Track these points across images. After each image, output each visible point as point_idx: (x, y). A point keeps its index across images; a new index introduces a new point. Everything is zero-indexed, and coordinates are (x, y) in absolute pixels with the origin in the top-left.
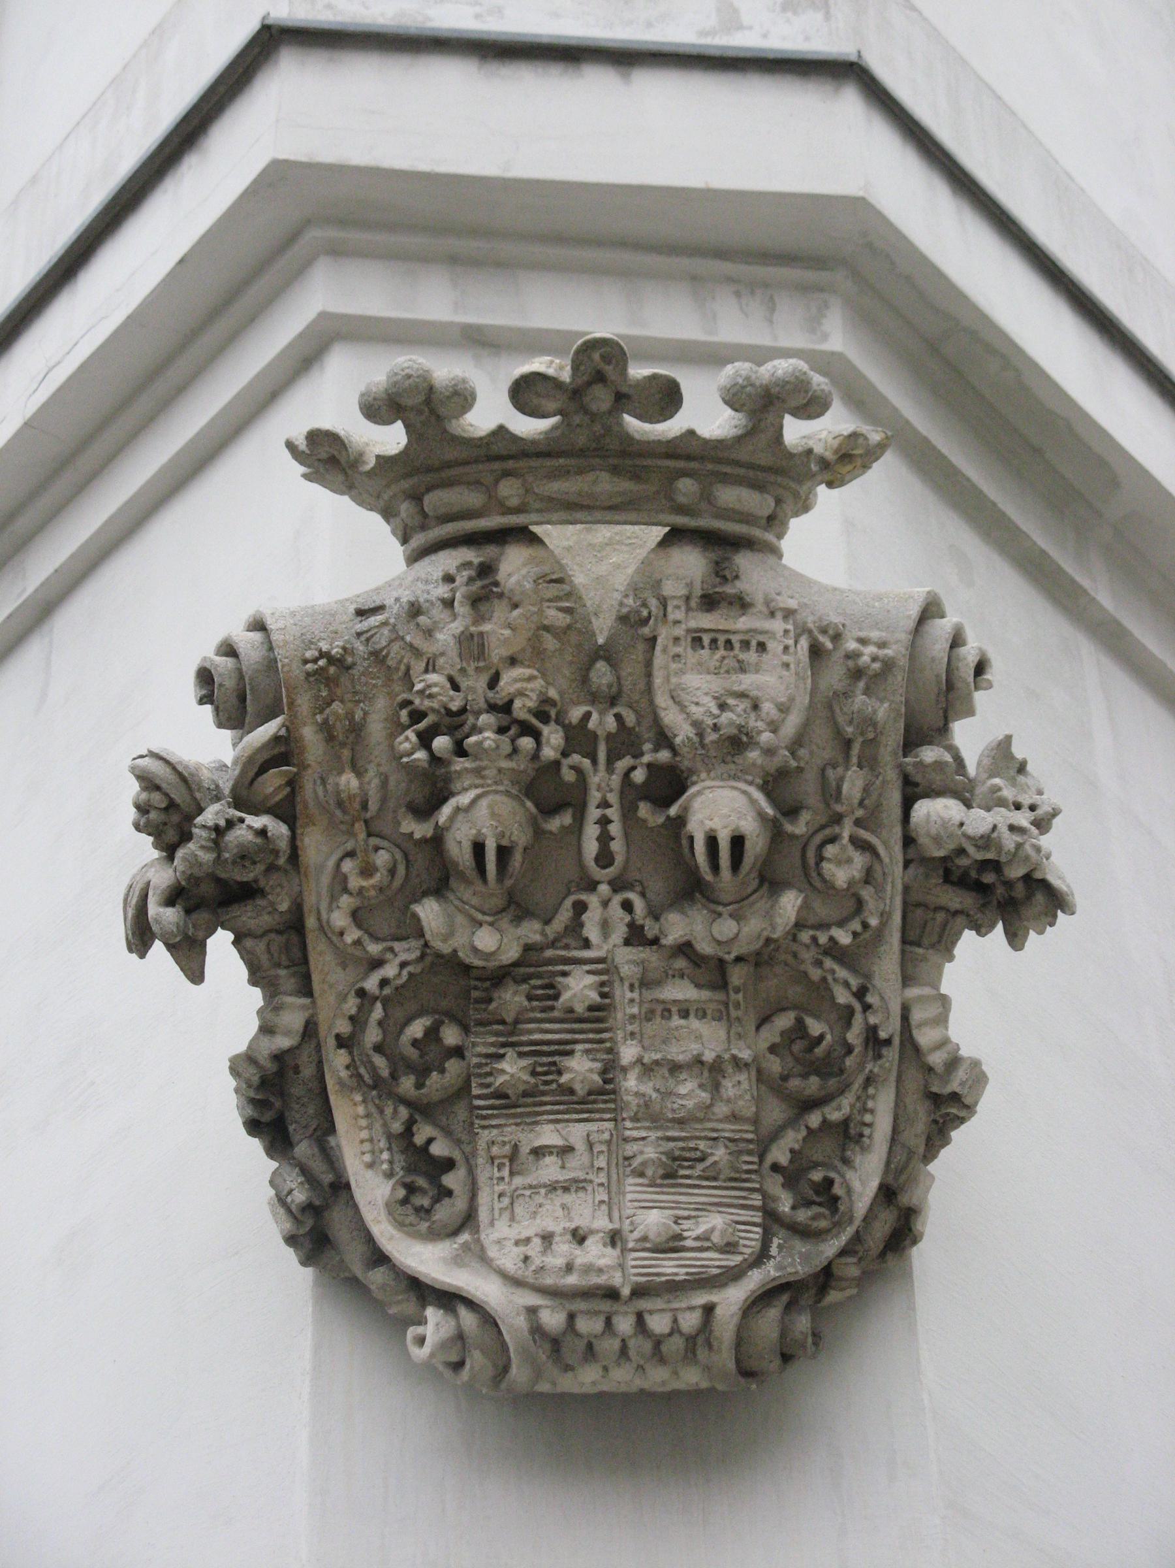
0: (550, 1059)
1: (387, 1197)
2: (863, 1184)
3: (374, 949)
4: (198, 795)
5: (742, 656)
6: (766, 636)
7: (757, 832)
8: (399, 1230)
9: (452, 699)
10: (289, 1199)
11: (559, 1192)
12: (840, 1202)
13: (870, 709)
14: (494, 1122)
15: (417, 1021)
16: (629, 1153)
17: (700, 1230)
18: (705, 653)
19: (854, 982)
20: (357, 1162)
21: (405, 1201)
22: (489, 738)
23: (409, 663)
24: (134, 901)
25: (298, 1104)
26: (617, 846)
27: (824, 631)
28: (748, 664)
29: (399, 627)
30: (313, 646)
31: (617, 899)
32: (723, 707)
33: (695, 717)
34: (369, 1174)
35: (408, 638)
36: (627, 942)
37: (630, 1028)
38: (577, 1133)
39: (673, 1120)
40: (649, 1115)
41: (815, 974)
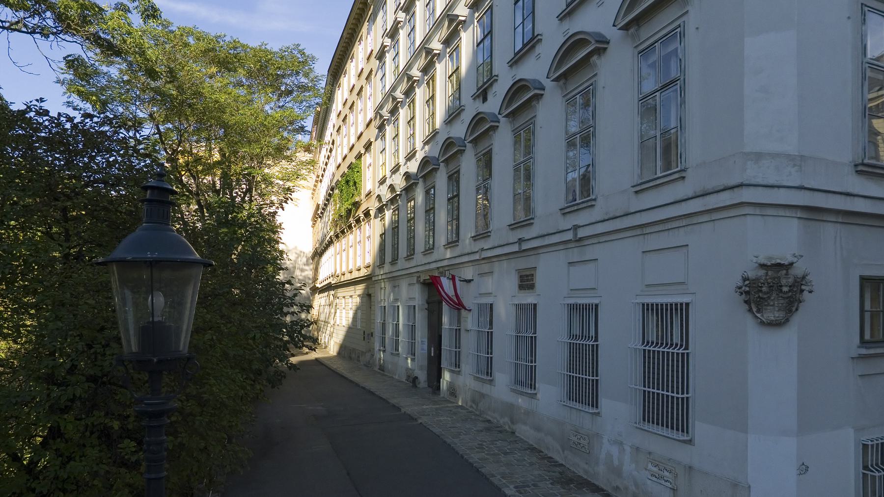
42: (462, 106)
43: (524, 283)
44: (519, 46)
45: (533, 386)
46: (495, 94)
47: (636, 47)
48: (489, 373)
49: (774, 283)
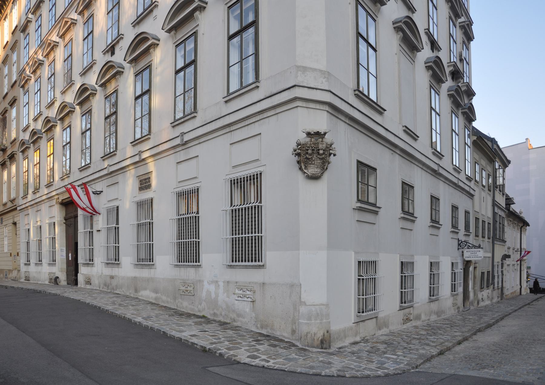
38: (313, 166)
42: (94, 60)
43: (143, 185)
44: (141, 10)
45: (151, 259)
46: (121, 48)
47: (226, 4)
48: (117, 259)
49: (315, 148)
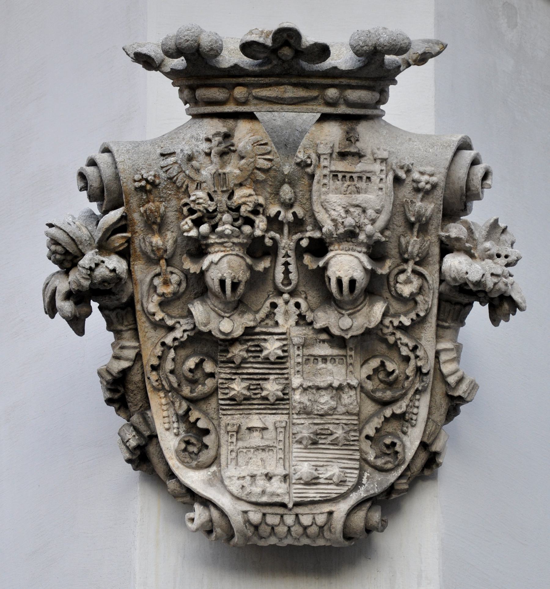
0: (257, 382)
1: (176, 447)
2: (412, 443)
3: (170, 322)
4: (80, 247)
5: (358, 185)
6: (371, 174)
7: (363, 278)
8: (182, 464)
9: (209, 206)
10: (128, 444)
11: (260, 451)
12: (399, 455)
13: (423, 210)
14: (229, 412)
15: (192, 359)
16: (295, 431)
17: (328, 475)
18: (339, 183)
19: (411, 344)
20: (161, 427)
21: (185, 450)
22: (227, 228)
23: (188, 184)
24: (49, 294)
25: (132, 393)
26: (293, 276)
27: (402, 168)
28: (362, 189)
29: (182, 166)
30: (138, 172)
31: (292, 302)
32: (347, 212)
33: (333, 217)
34: (167, 433)
35: (187, 172)
36: (297, 324)
37: (297, 369)
38: (270, 420)
39: (317, 415)
40: (306, 412)
41: (391, 339)
